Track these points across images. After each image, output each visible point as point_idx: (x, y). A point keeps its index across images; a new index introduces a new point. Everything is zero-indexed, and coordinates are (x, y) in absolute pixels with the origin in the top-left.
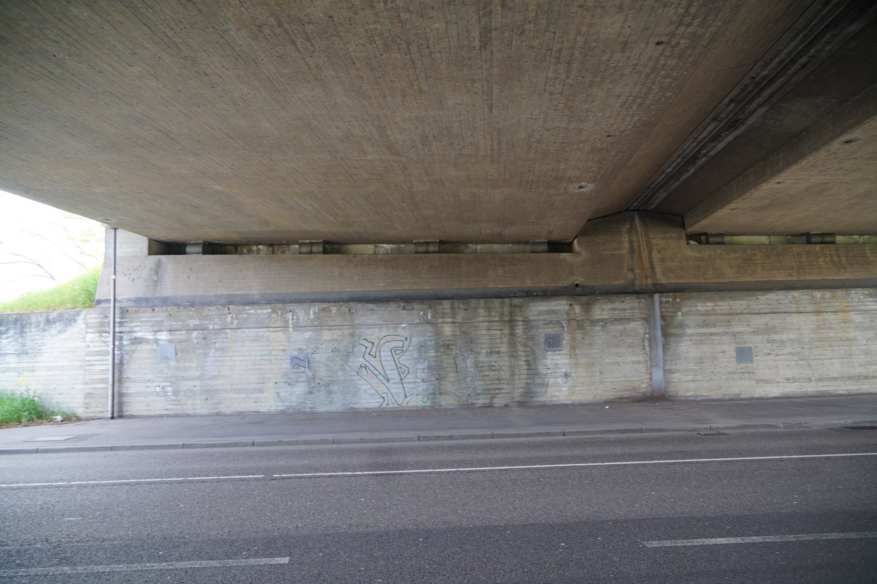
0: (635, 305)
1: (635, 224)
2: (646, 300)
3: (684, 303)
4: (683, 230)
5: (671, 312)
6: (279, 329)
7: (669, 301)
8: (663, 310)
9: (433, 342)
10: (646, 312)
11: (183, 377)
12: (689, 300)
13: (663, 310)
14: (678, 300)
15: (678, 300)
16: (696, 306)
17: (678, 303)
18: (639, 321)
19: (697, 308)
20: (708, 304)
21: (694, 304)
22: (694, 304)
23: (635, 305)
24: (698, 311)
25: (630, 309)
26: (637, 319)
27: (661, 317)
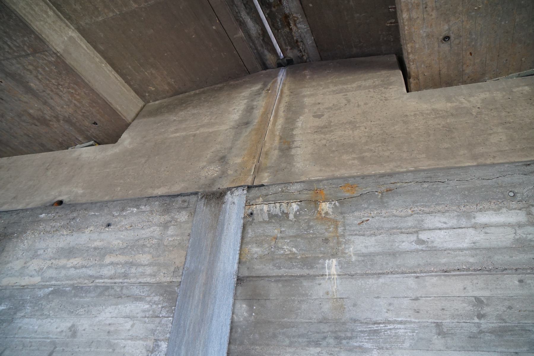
0: (146, 233)
1: (276, 82)
2: (193, 214)
3: (353, 219)
4: (277, 66)
5: (291, 258)
6: (520, 164)
7: (286, 215)
8: (255, 250)
9: (300, 218)
10: (179, 262)
11: (34, 259)
12: (382, 204)
13: (255, 250)
14: (325, 207)
15: (325, 207)
16: (418, 229)
17: (325, 219)
18: (138, 299)
19: (423, 236)
20: (482, 218)
21: (410, 222)
22: (410, 222)
23: (146, 233)
24: (434, 250)
25: (122, 251)
26: (136, 291)
27: (240, 280)
